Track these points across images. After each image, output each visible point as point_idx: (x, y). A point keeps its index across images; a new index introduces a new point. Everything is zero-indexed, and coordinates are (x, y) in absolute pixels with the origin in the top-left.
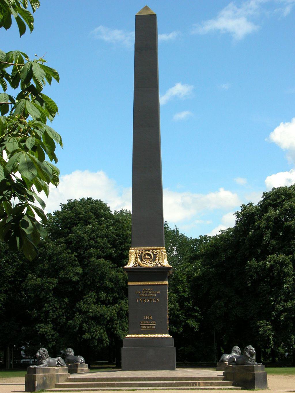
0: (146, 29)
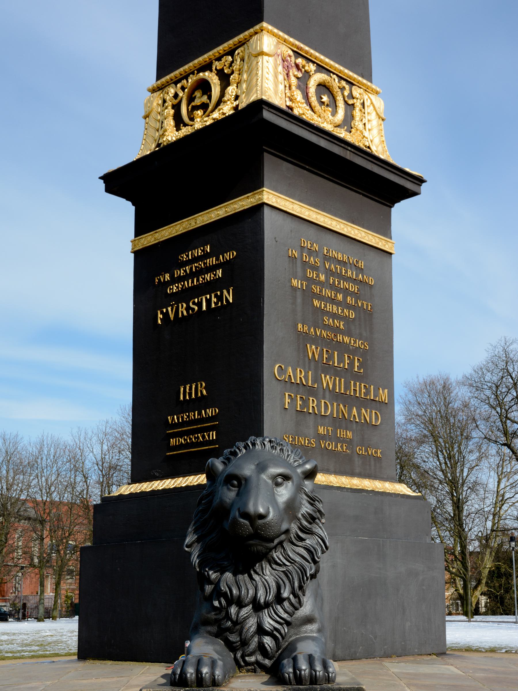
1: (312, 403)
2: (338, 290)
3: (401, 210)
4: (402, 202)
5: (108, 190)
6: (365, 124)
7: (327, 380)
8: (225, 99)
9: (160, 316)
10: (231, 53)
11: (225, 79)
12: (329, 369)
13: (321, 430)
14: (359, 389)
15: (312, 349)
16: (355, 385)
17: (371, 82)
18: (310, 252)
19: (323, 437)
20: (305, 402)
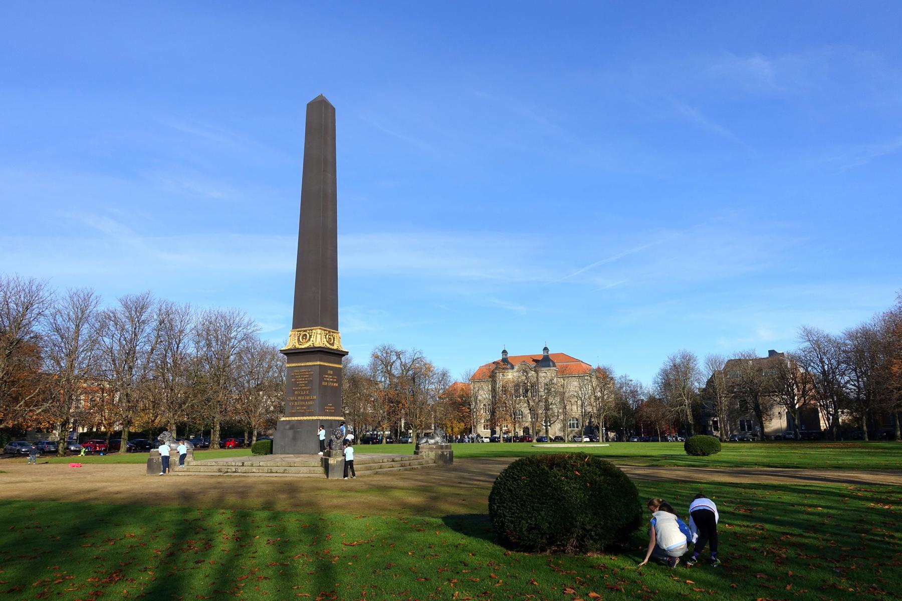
0: (320, 122)
5: (310, 106)
7: (300, 398)
12: (300, 395)
14: (308, 398)
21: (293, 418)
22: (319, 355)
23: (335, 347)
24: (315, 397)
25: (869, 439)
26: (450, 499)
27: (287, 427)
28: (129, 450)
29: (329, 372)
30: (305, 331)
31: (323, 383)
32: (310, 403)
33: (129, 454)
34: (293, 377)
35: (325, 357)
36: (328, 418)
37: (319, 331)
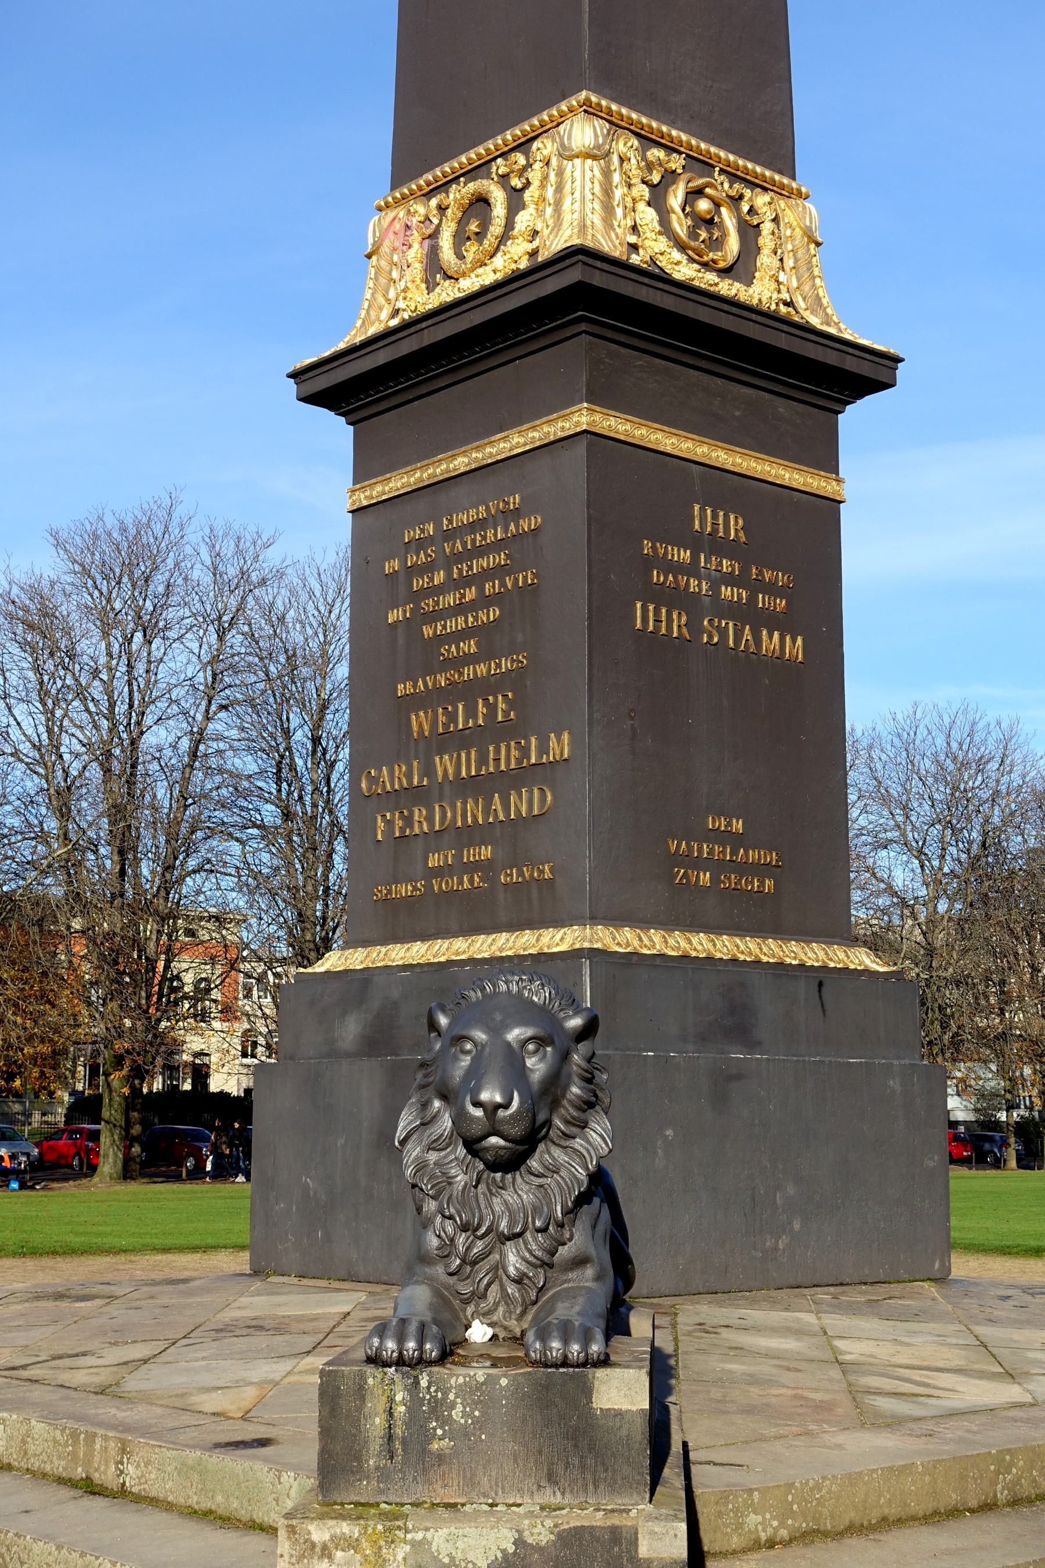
1: (418, 814)
2: (466, 582)
3: (856, 420)
4: (867, 397)
6: (781, 260)
7: (444, 765)
8: (516, 232)
9: (455, 570)
10: (524, 145)
11: (516, 200)
12: (450, 741)
13: (434, 861)
14: (506, 756)
15: (419, 722)
16: (497, 751)
17: (794, 178)
18: (420, 544)
19: (438, 872)
20: (409, 821)
21: (398, 954)
22: (576, 352)
23: (760, 292)
24: (561, 746)
25: (1020, 1166)
26: (690, 253)
27: (350, 1030)
28: (128, 1172)
29: (702, 518)
30: (478, 170)
31: (643, 615)
32: (524, 803)
33: (136, 1188)
34: (396, 590)
35: (643, 369)
36: (701, 944)
37: (583, 133)
